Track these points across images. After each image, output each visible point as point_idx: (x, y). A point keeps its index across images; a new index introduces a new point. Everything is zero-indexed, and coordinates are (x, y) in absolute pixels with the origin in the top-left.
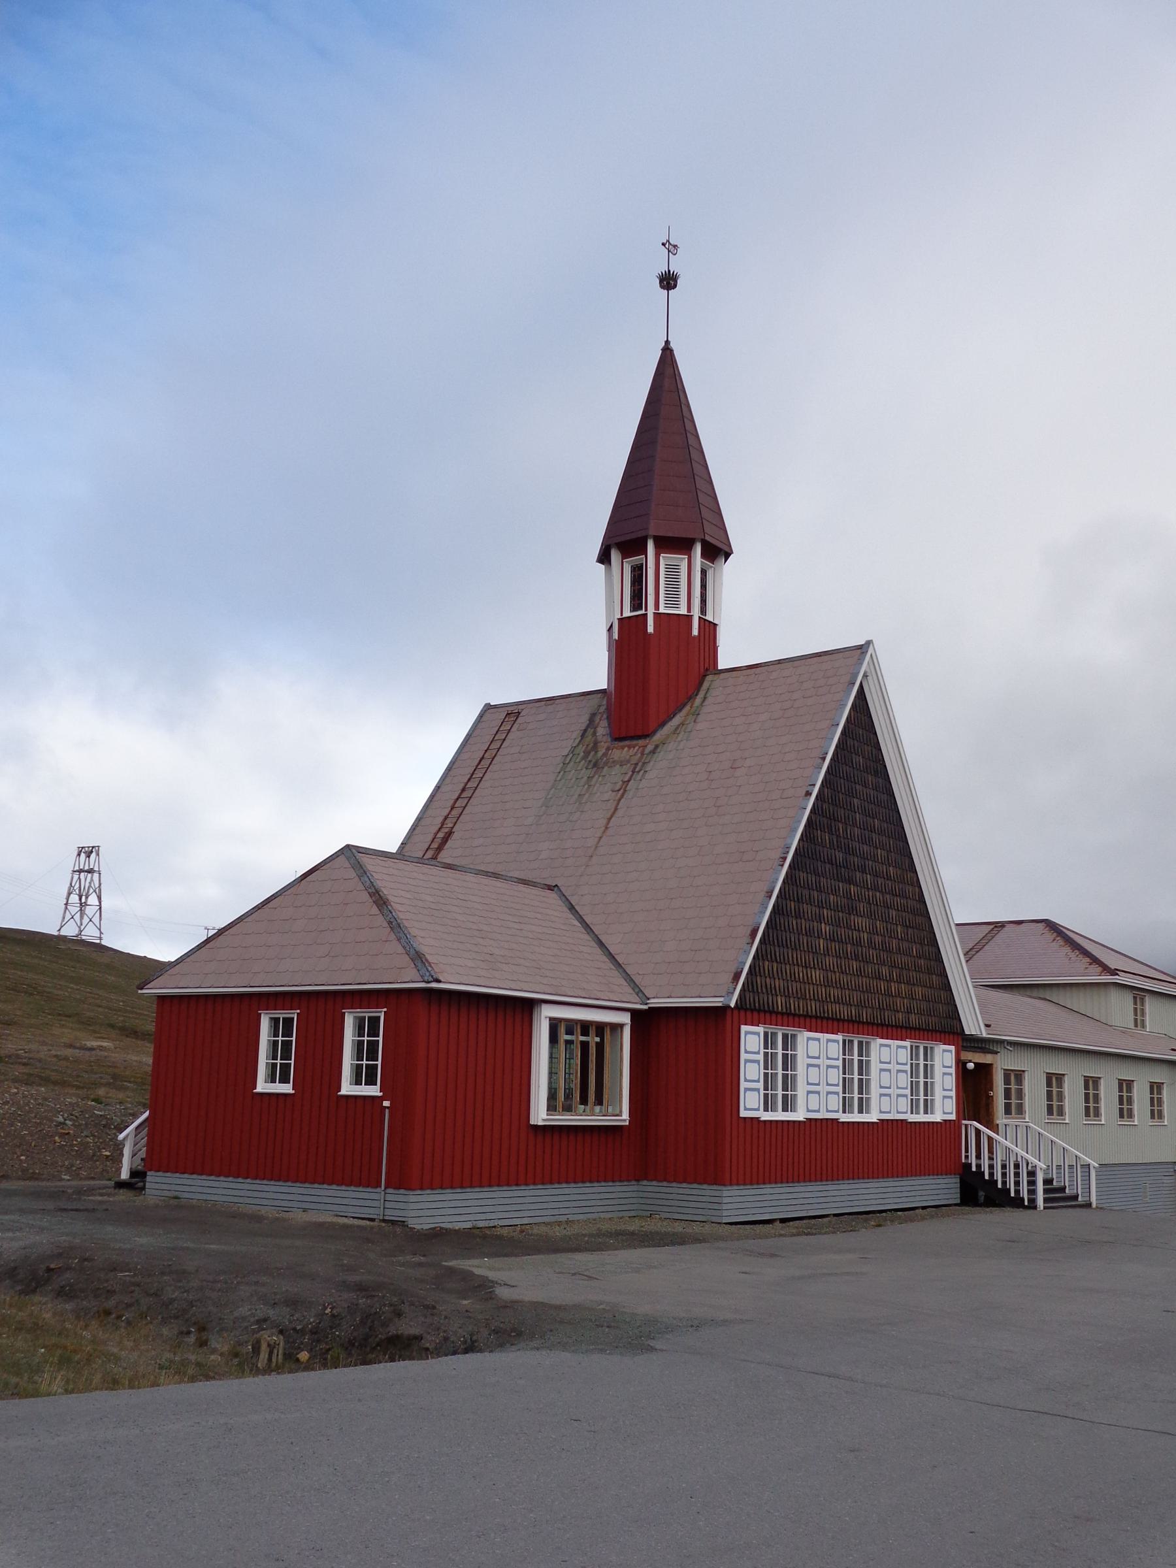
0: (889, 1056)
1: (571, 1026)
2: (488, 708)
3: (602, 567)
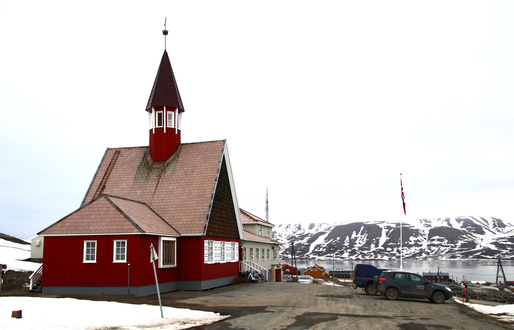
0: (228, 245)
2: (108, 149)
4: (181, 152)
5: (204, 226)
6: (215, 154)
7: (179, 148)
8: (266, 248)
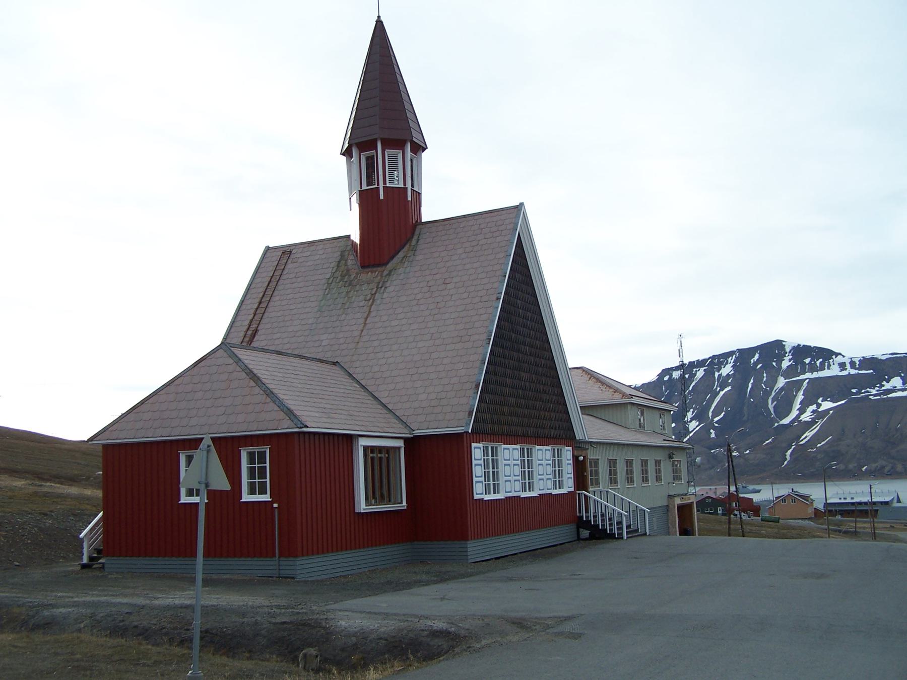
0: (542, 454)
1: (373, 449)
2: (268, 249)
3: (344, 158)
4: (421, 241)
5: (467, 408)
6: (498, 239)
7: (417, 232)
8: (651, 457)
